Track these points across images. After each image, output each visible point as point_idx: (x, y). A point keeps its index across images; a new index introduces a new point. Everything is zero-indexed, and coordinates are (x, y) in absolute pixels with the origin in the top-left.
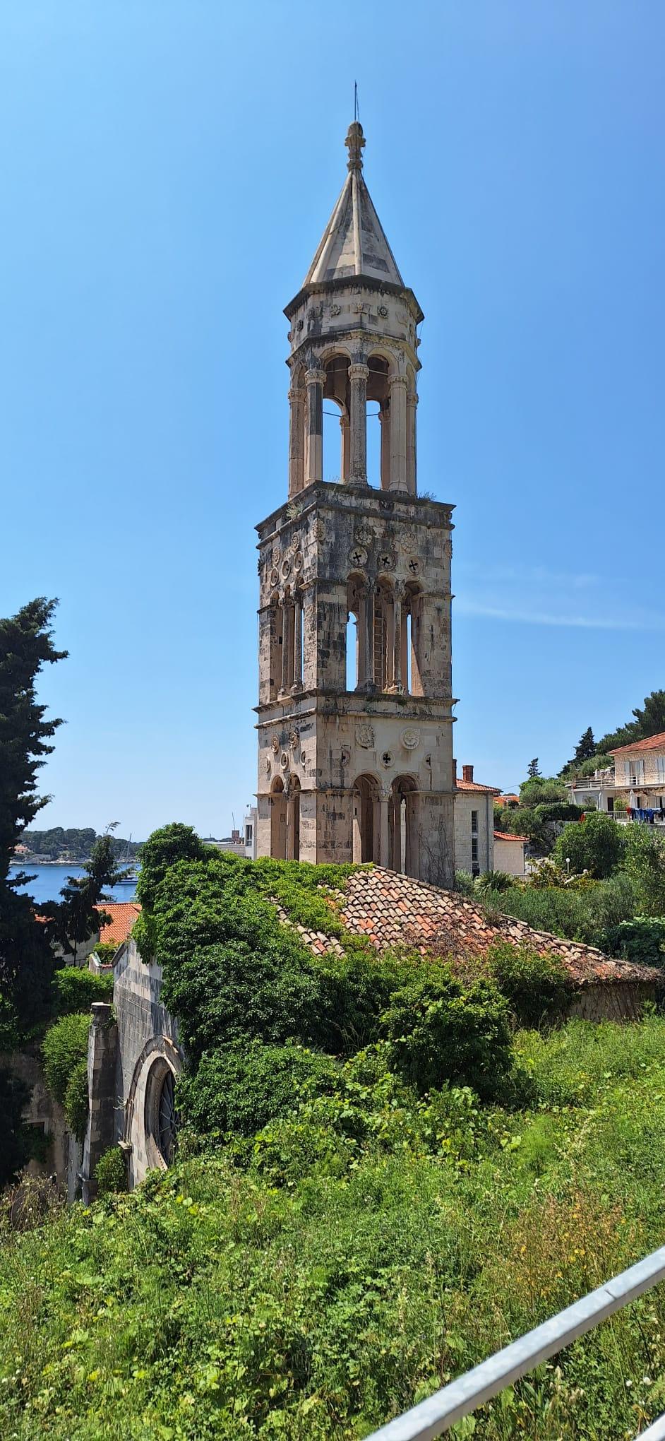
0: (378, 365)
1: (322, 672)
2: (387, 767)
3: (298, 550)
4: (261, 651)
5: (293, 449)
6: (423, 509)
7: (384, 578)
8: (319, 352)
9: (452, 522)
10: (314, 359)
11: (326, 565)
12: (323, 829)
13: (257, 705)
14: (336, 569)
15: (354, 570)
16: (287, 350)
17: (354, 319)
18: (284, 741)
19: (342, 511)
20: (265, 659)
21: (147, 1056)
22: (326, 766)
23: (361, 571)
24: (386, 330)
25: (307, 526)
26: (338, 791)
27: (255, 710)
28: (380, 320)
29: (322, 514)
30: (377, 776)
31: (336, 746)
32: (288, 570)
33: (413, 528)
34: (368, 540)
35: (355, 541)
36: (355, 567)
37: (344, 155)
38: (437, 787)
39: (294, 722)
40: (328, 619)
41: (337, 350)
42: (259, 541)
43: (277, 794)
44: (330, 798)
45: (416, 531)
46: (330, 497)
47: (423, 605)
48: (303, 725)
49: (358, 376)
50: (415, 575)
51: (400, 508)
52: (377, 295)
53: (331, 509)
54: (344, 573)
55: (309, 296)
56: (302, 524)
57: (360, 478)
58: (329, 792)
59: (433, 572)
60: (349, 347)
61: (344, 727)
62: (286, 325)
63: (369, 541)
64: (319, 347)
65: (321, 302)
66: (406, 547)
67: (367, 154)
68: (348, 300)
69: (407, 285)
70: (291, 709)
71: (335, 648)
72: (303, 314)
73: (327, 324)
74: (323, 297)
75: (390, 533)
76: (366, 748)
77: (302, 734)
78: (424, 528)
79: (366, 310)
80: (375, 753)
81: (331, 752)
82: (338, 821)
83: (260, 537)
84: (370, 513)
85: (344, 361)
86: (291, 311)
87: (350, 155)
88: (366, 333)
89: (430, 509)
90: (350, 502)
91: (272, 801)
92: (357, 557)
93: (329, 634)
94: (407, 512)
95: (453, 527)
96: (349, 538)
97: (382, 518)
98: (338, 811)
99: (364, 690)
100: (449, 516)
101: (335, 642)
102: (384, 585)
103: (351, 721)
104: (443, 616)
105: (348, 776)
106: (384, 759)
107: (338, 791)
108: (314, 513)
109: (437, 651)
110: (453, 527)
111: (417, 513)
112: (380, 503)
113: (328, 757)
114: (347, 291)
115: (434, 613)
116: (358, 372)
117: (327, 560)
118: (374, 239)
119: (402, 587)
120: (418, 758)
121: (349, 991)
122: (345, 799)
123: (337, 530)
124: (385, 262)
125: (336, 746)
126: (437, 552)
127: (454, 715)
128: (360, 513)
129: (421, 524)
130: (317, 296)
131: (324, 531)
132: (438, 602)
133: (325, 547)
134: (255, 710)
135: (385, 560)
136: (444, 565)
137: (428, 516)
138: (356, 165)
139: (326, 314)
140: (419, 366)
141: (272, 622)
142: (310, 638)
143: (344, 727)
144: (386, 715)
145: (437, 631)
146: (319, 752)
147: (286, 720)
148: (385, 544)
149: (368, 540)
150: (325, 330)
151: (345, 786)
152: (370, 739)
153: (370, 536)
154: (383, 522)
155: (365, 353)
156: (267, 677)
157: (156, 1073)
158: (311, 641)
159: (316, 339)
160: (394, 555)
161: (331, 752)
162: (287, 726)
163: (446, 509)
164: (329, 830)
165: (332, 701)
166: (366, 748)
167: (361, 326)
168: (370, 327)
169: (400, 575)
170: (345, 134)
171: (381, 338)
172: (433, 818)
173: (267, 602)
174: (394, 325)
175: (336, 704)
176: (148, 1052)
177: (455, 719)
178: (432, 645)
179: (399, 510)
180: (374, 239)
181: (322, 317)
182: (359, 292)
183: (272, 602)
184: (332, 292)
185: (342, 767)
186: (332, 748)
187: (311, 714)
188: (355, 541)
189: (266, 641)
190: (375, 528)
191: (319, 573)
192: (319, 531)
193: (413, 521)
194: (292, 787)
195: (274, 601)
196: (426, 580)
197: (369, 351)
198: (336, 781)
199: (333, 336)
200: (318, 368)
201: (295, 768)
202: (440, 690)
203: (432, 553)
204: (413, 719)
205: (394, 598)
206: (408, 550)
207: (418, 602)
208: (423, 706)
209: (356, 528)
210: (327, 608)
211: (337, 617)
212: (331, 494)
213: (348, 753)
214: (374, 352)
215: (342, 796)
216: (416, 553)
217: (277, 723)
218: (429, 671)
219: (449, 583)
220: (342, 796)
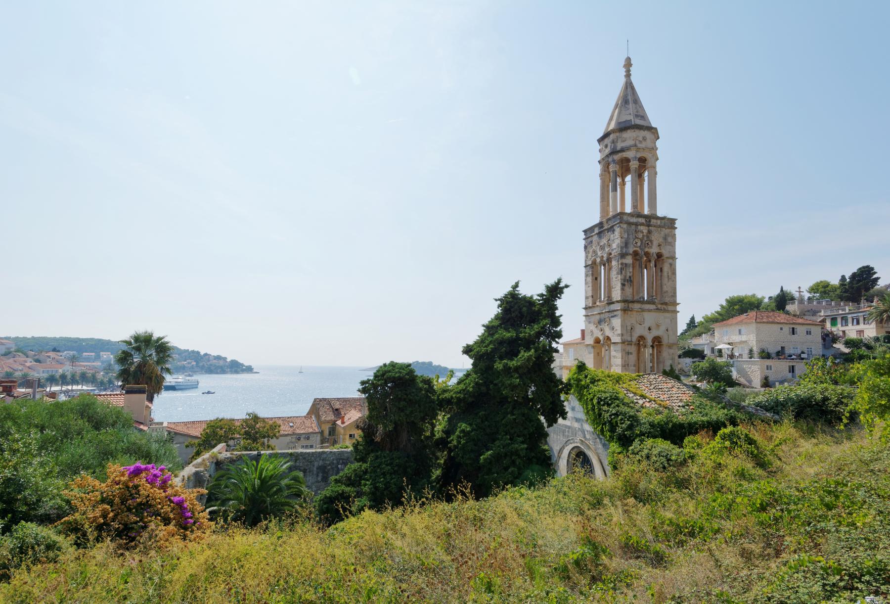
8: (617, 157)
19: (630, 224)
37: (623, 72)
50: (660, 249)
66: (656, 238)
68: (629, 134)
73: (619, 146)
74: (618, 134)
75: (649, 232)
84: (642, 224)
114: (629, 131)
120: (663, 328)
126: (670, 239)
138: (628, 75)
139: (619, 141)
144: (649, 311)
170: (623, 63)
172: (669, 355)
196: (665, 252)
197: (639, 155)
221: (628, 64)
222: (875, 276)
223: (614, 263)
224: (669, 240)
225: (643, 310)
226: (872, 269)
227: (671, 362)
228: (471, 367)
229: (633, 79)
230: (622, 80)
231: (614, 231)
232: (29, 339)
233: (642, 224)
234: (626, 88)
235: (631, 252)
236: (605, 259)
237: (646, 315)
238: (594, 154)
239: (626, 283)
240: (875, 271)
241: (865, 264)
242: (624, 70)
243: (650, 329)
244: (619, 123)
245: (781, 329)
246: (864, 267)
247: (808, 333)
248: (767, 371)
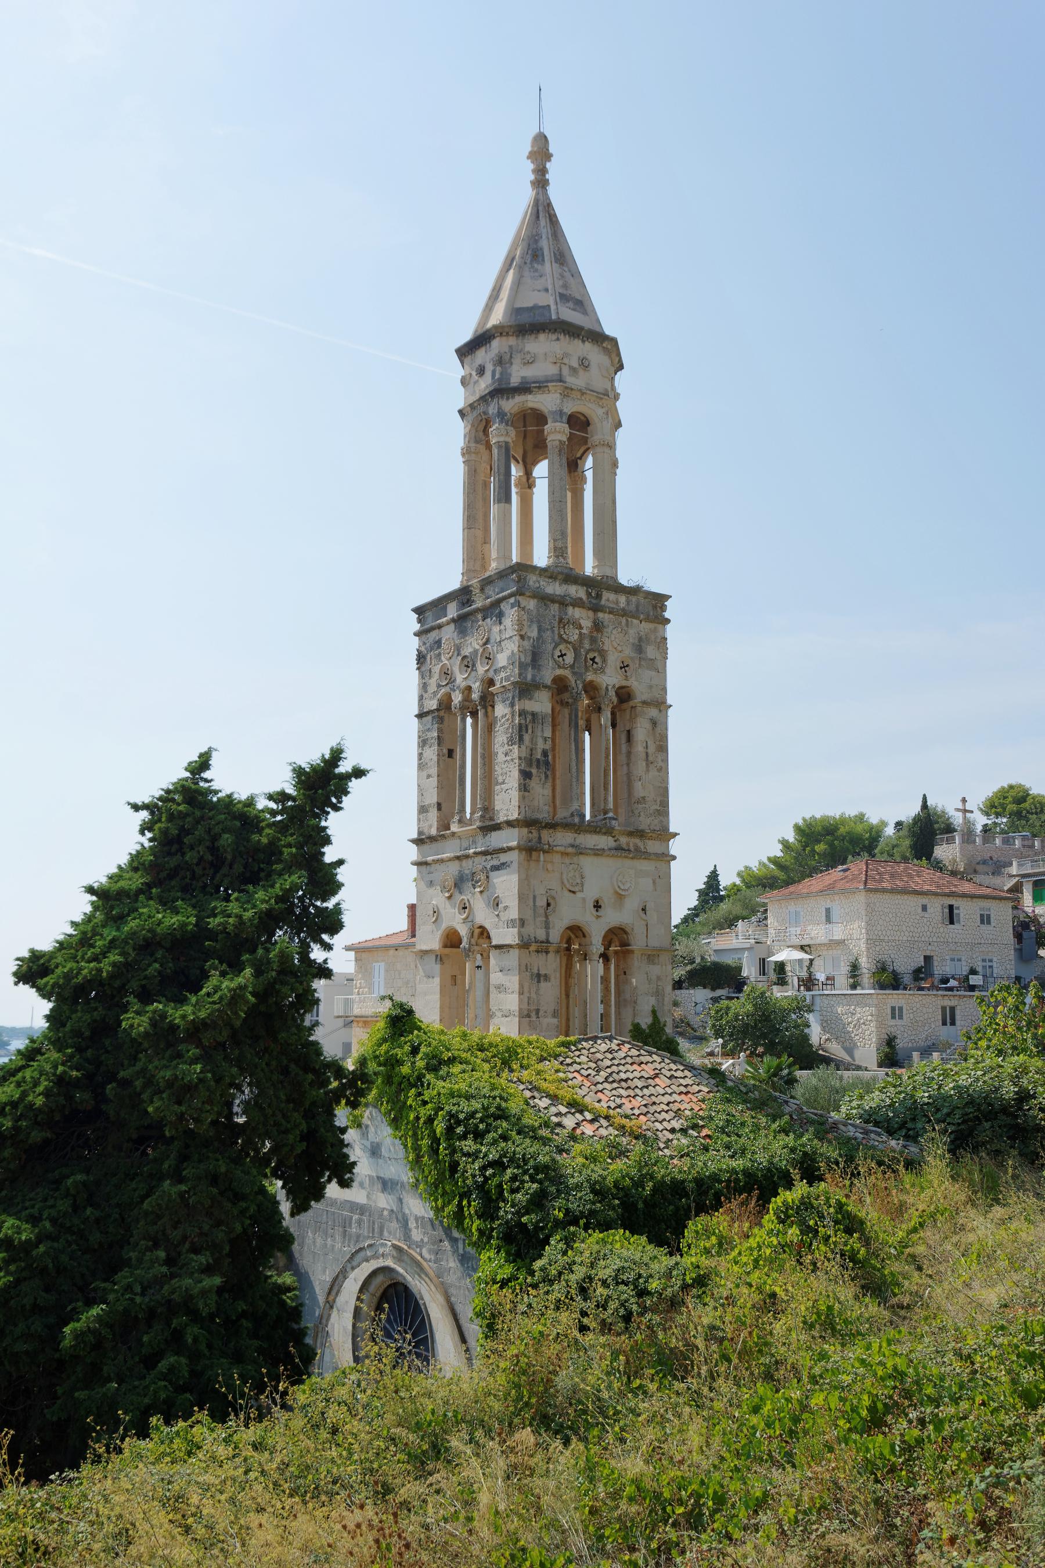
0: (579, 423)
1: (524, 797)
2: (598, 917)
3: (485, 644)
4: (421, 766)
5: (469, 517)
6: (634, 599)
7: (591, 682)
8: (511, 405)
9: (667, 615)
10: (501, 414)
11: (527, 665)
12: (526, 995)
13: (415, 836)
14: (539, 670)
15: (559, 672)
16: (459, 398)
17: (552, 370)
18: (459, 883)
19: (545, 599)
20: (429, 776)
21: (353, 1268)
22: (528, 915)
23: (567, 673)
24: (588, 384)
25: (500, 616)
26: (543, 947)
27: (413, 841)
28: (581, 372)
29: (523, 603)
30: (586, 929)
31: (541, 890)
32: (468, 664)
33: (624, 620)
34: (574, 635)
35: (560, 636)
36: (559, 667)
37: (527, 169)
38: (654, 943)
39: (479, 859)
40: (530, 731)
41: (530, 405)
42: (417, 627)
43: (448, 950)
44: (534, 954)
45: (627, 625)
46: (531, 583)
47: (636, 716)
48: (495, 862)
49: (559, 437)
50: (626, 678)
51: (608, 597)
52: (577, 343)
53: (534, 597)
54: (548, 675)
55: (494, 338)
56: (494, 611)
57: (561, 560)
58: (533, 948)
59: (647, 674)
60: (546, 402)
61: (549, 866)
62: (456, 370)
63: (576, 637)
64: (508, 399)
65: (511, 347)
67: (553, 168)
68: (542, 345)
69: (609, 331)
70: (474, 842)
71: (538, 767)
72: (482, 356)
73: (517, 374)
74: (512, 341)
75: (598, 626)
76: (574, 892)
77: (492, 874)
78: (636, 621)
79: (566, 361)
80: (584, 899)
81: (535, 897)
82: (543, 984)
83: (419, 621)
84: (577, 603)
85: (539, 418)
86: (465, 352)
87: (534, 171)
88: (566, 388)
89: (642, 601)
90: (555, 588)
91: (440, 959)
92: (562, 656)
93: (531, 750)
94: (617, 603)
95: (668, 621)
96: (553, 632)
97: (589, 609)
98: (542, 972)
99: (569, 820)
100: (663, 608)
101: (538, 760)
102: (591, 689)
103: (557, 858)
104: (658, 730)
105: (554, 927)
106: (595, 906)
107: (543, 947)
108: (512, 600)
109: (653, 773)
110: (668, 621)
111: (628, 602)
112: (587, 591)
113: (531, 904)
114: (542, 337)
115: (648, 725)
116: (556, 432)
117: (529, 659)
118: (567, 275)
119: (612, 693)
120: (632, 904)
121: (533, 1211)
122: (551, 955)
123: (539, 622)
124: (582, 304)
125: (541, 890)
126: (651, 652)
127: (672, 852)
128: (563, 602)
129: (633, 617)
130: (504, 339)
131: (525, 623)
132: (653, 712)
133: (526, 643)
134: (413, 841)
135: (593, 660)
136: (658, 666)
137: (640, 608)
138: (541, 182)
139: (517, 361)
140: (619, 425)
141: (440, 730)
142: (506, 755)
143: (549, 866)
144: (598, 852)
145: (652, 749)
146: (522, 898)
147: (467, 857)
148: (593, 640)
149: (574, 635)
150: (515, 381)
151: (551, 939)
152: (579, 881)
153: (577, 631)
154: (591, 613)
155: (565, 410)
156: (432, 798)
157: (372, 1288)
158: (508, 758)
159: (501, 391)
160: (603, 653)
161: (535, 897)
162: (467, 865)
163: (659, 600)
164: (533, 995)
165: (535, 834)
166: (574, 892)
167: (561, 380)
168: (571, 380)
169: (609, 679)
170: (527, 148)
171: (583, 394)
172: (650, 981)
173: (433, 704)
174: (594, 378)
175: (540, 838)
176: (354, 1263)
177: (674, 858)
178: (647, 765)
179: (608, 600)
180: (567, 275)
181: (512, 364)
182: (558, 339)
183: (440, 704)
184: (524, 335)
185: (547, 916)
186: (537, 893)
187: (510, 849)
188: (560, 636)
189: (431, 753)
190: (582, 621)
191: (520, 675)
192: (520, 624)
193: (624, 613)
194: (473, 941)
195: (445, 705)
196: (640, 690)
197: (570, 408)
198: (541, 934)
199: (524, 388)
200: (507, 425)
201: (483, 915)
202: (656, 821)
203: (646, 653)
204: (626, 857)
205: (603, 706)
206: (619, 648)
207: (628, 712)
208: (637, 841)
209: (561, 620)
210: (529, 718)
211: (540, 729)
212: (532, 580)
213: (554, 898)
214: (574, 410)
215: (547, 952)
216: (627, 652)
217: (450, 860)
218: (644, 798)
219: (664, 689)
220: (547, 952)
225: (580, 851)
227: (652, 1001)
229: (555, 194)
230: (526, 195)
233: (577, 603)
234: (536, 215)
236: (475, 696)
237: (587, 863)
239: (534, 771)
244: (515, 311)
245: (924, 908)
247: (985, 919)
248: (893, 1022)
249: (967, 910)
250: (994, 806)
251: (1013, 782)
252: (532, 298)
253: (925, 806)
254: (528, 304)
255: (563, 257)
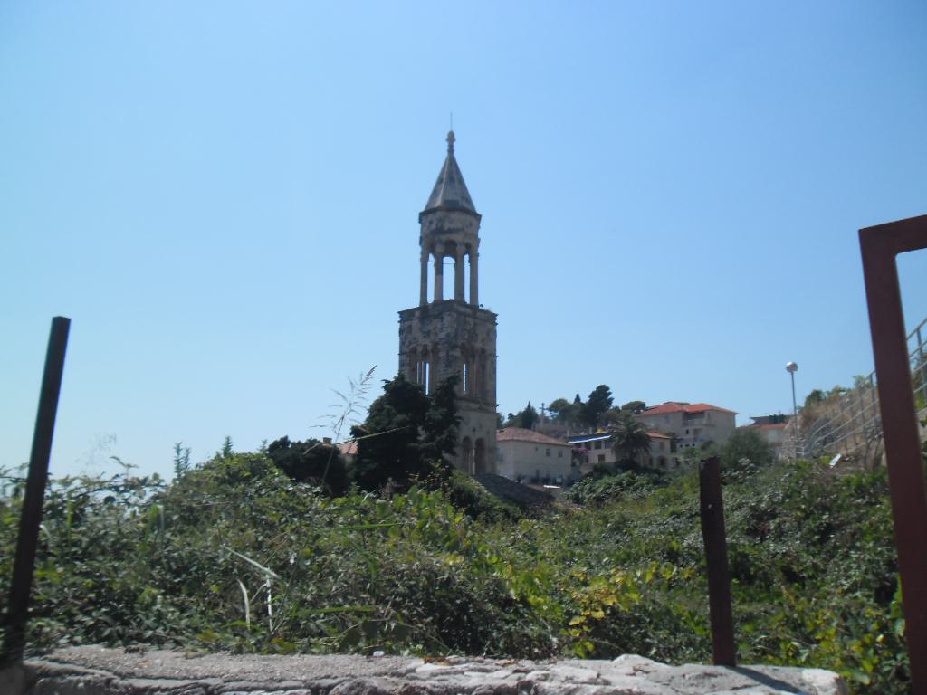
8: (444, 238)
19: (460, 314)
37: (446, 146)
67: (456, 145)
68: (456, 216)
72: (430, 217)
73: (447, 226)
75: (475, 324)
84: (469, 316)
124: (468, 200)
138: (451, 151)
144: (474, 410)
160: (477, 335)
170: (446, 137)
196: (487, 348)
197: (466, 241)
199: (450, 231)
221: (451, 138)
222: (610, 396)
223: (442, 354)
224: (491, 335)
226: (608, 389)
228: (498, 411)
229: (457, 155)
230: (444, 155)
231: (442, 318)
232: (477, 251)
233: (469, 316)
234: (450, 164)
235: (460, 344)
236: (429, 348)
238: (415, 230)
240: (610, 391)
241: (558, 398)
242: (447, 144)
243: (474, 430)
244: (445, 202)
245: (537, 449)
246: (560, 400)
247: (560, 455)
249: (555, 451)
250: (554, 407)
251: (554, 400)
252: (451, 197)
253: (529, 406)
254: (450, 199)
255: (461, 181)
